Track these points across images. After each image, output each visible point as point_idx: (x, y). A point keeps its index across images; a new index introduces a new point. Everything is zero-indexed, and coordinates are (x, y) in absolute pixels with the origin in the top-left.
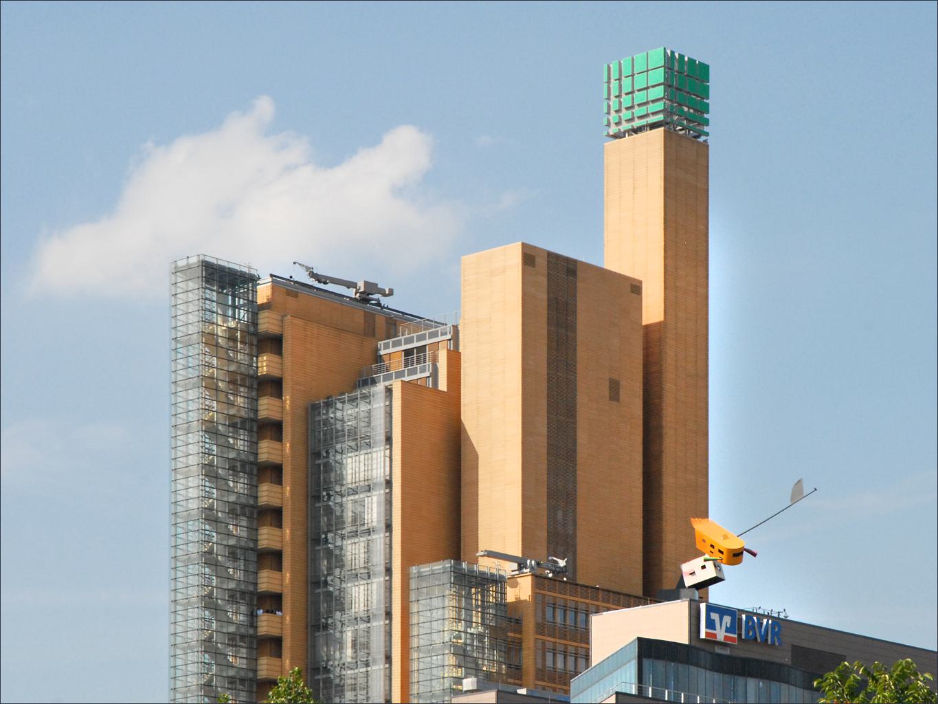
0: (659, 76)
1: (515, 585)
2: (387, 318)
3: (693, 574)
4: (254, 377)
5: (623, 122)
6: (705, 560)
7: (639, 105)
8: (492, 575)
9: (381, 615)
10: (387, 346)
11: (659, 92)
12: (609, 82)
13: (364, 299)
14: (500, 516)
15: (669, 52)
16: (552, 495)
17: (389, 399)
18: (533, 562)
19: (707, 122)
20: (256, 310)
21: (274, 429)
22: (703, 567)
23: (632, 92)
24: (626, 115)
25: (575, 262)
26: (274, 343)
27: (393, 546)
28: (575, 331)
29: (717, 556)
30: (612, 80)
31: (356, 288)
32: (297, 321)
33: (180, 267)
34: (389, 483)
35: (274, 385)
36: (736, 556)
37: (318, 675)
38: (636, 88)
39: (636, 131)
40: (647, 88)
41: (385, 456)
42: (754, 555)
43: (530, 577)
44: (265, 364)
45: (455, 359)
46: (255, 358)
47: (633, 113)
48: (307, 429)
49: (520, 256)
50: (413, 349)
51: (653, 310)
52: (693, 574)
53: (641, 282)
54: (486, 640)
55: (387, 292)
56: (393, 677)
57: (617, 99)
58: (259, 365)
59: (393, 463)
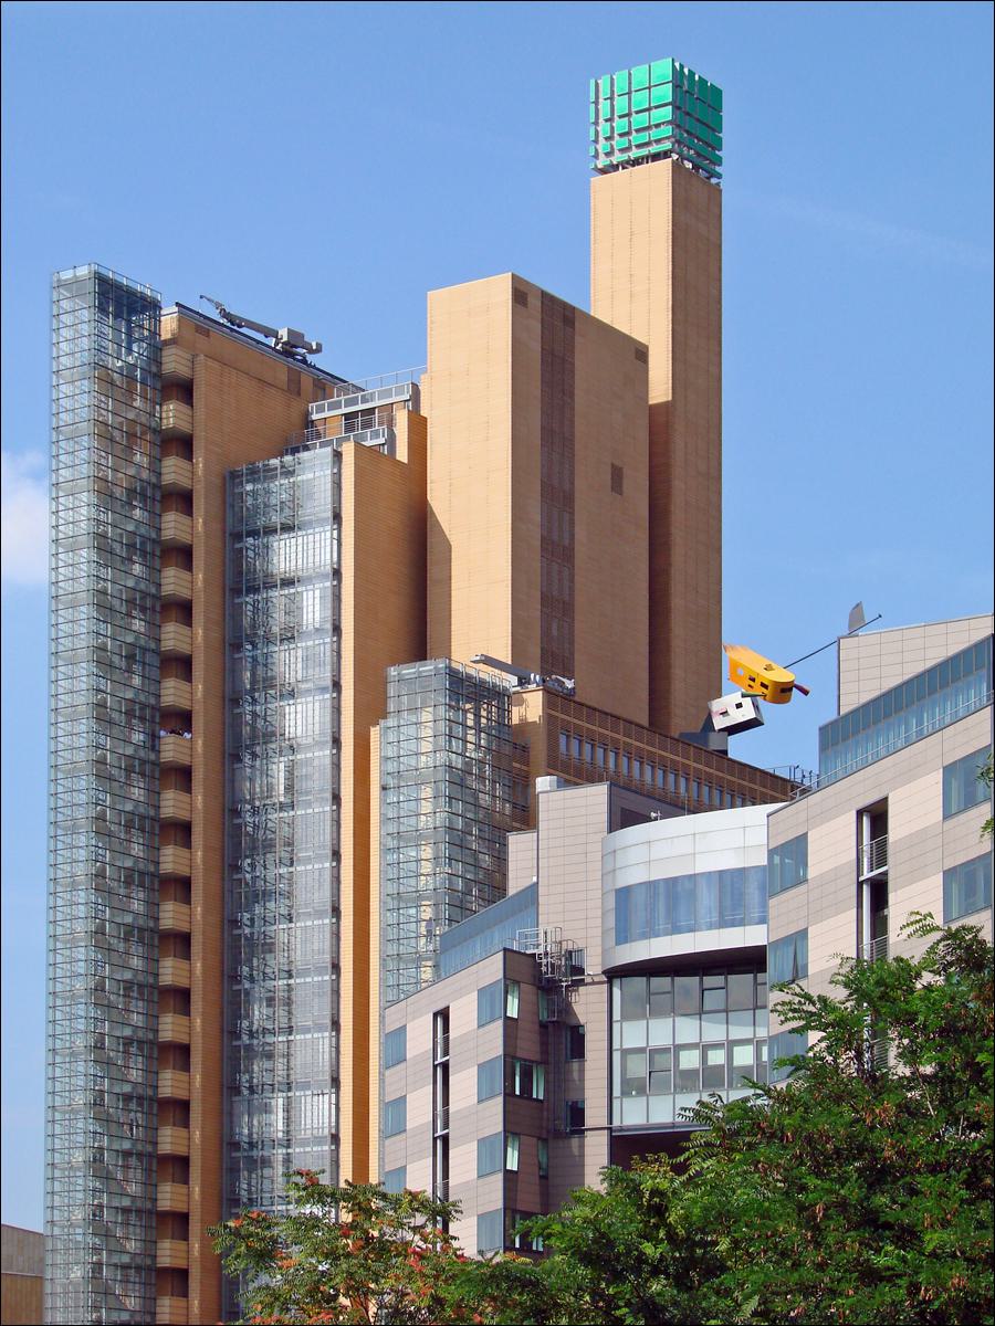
0: (666, 93)
1: (521, 702)
2: (314, 379)
3: (725, 713)
4: (156, 431)
5: (616, 152)
6: (744, 696)
7: (638, 131)
8: (494, 685)
9: (327, 742)
10: (320, 409)
11: (666, 113)
12: (596, 103)
13: (288, 351)
14: (482, 617)
15: (677, 65)
16: (546, 600)
17: (337, 466)
18: (538, 677)
19: (719, 162)
20: (157, 348)
21: (183, 500)
22: (739, 706)
23: (629, 115)
24: (619, 143)
25: (573, 309)
26: (183, 390)
27: (343, 653)
28: (572, 395)
29: (759, 690)
30: (600, 100)
31: (276, 337)
32: (210, 363)
33: (65, 281)
34: (337, 573)
35: (182, 444)
36: (783, 692)
37: (237, 818)
38: (634, 109)
39: (636, 162)
40: (649, 110)
41: (332, 538)
42: (805, 692)
43: (541, 692)
44: (171, 415)
45: (418, 426)
46: (158, 407)
47: (630, 141)
48: (224, 502)
49: (510, 290)
50: (358, 412)
51: (660, 387)
52: (725, 713)
53: (647, 347)
54: (487, 768)
55: (314, 347)
56: (342, 822)
57: (609, 124)
58: (164, 415)
59: (343, 547)
